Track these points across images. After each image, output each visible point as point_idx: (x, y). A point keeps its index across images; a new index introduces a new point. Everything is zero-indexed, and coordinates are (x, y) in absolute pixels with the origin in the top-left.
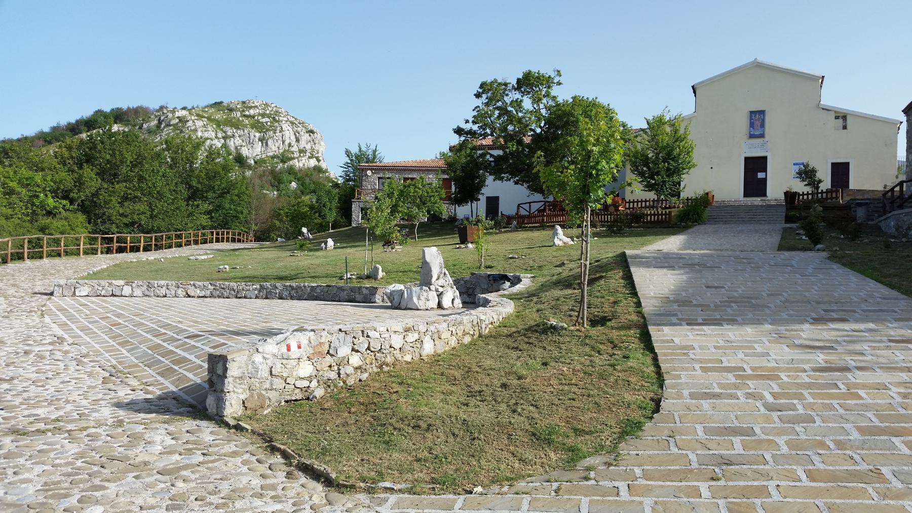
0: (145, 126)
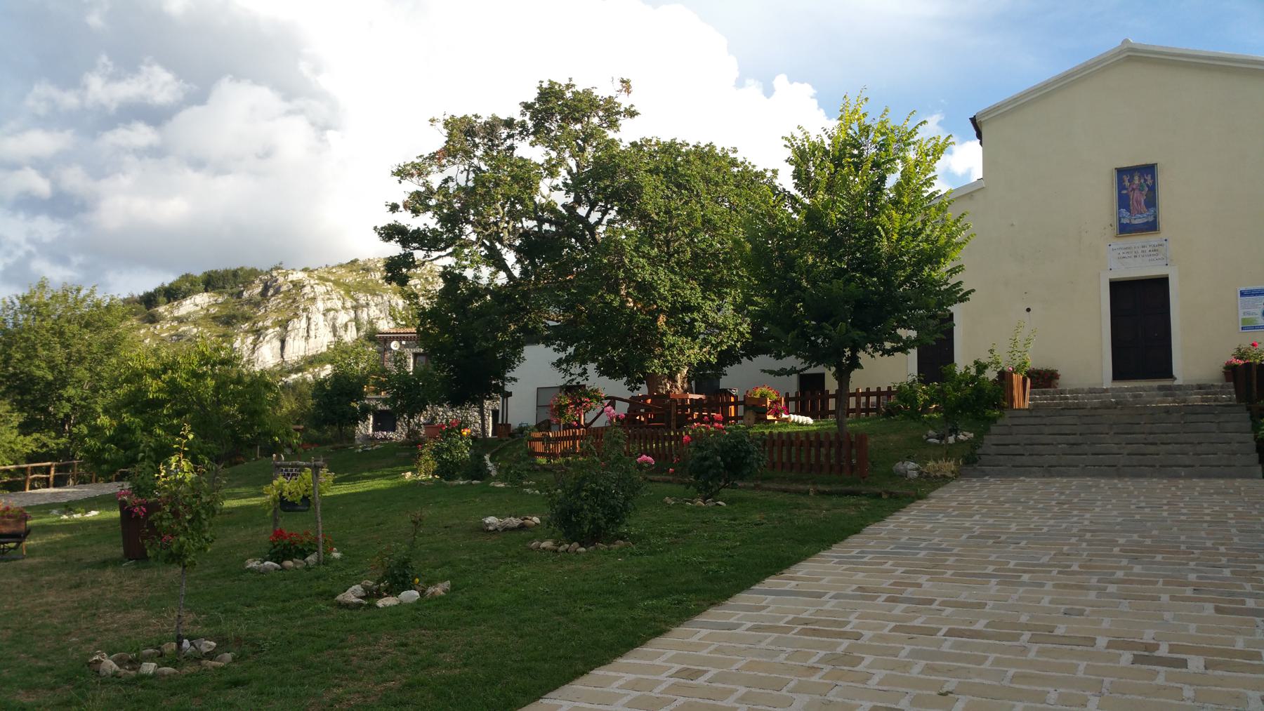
0: (246, 295)
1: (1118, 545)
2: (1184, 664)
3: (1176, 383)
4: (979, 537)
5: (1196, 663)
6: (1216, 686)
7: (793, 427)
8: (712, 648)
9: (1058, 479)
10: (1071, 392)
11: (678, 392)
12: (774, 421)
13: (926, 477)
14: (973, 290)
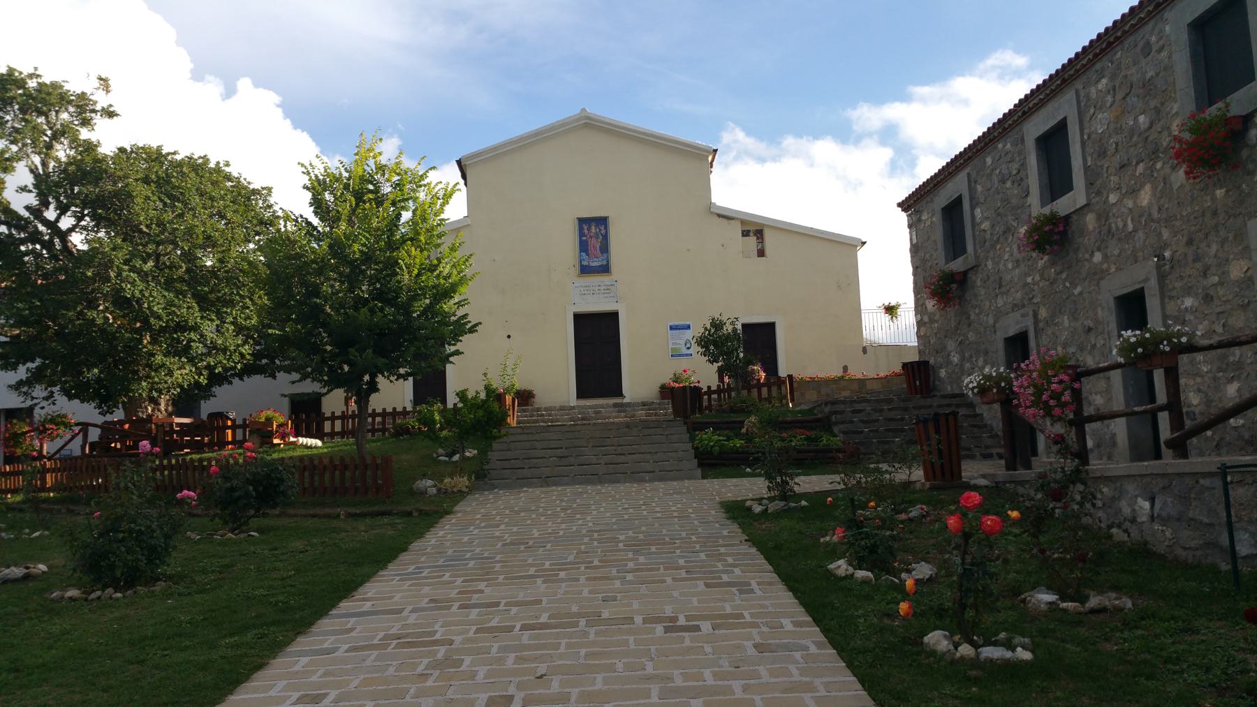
1: (621, 541)
2: (697, 628)
3: (626, 400)
4: (512, 543)
5: (706, 626)
6: (723, 641)
7: (302, 450)
8: (320, 673)
9: (554, 488)
10: (546, 409)
11: (161, 416)
12: (279, 444)
13: (445, 493)
14: (480, 323)
